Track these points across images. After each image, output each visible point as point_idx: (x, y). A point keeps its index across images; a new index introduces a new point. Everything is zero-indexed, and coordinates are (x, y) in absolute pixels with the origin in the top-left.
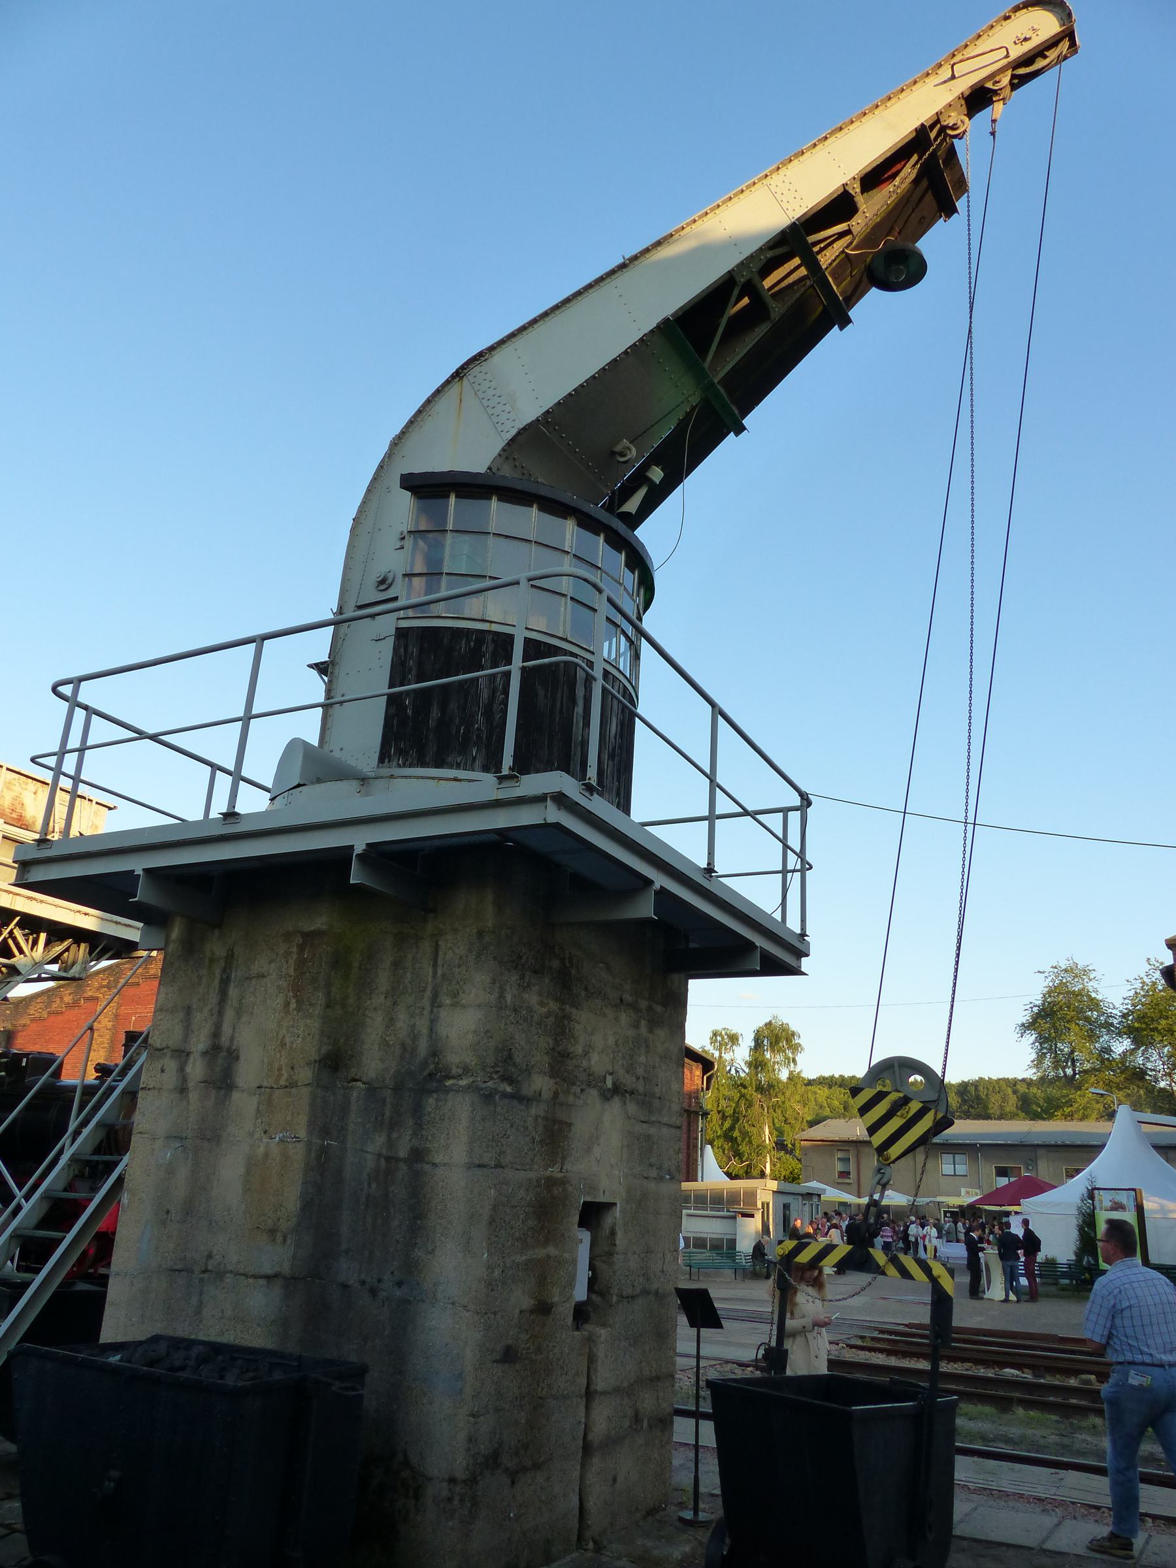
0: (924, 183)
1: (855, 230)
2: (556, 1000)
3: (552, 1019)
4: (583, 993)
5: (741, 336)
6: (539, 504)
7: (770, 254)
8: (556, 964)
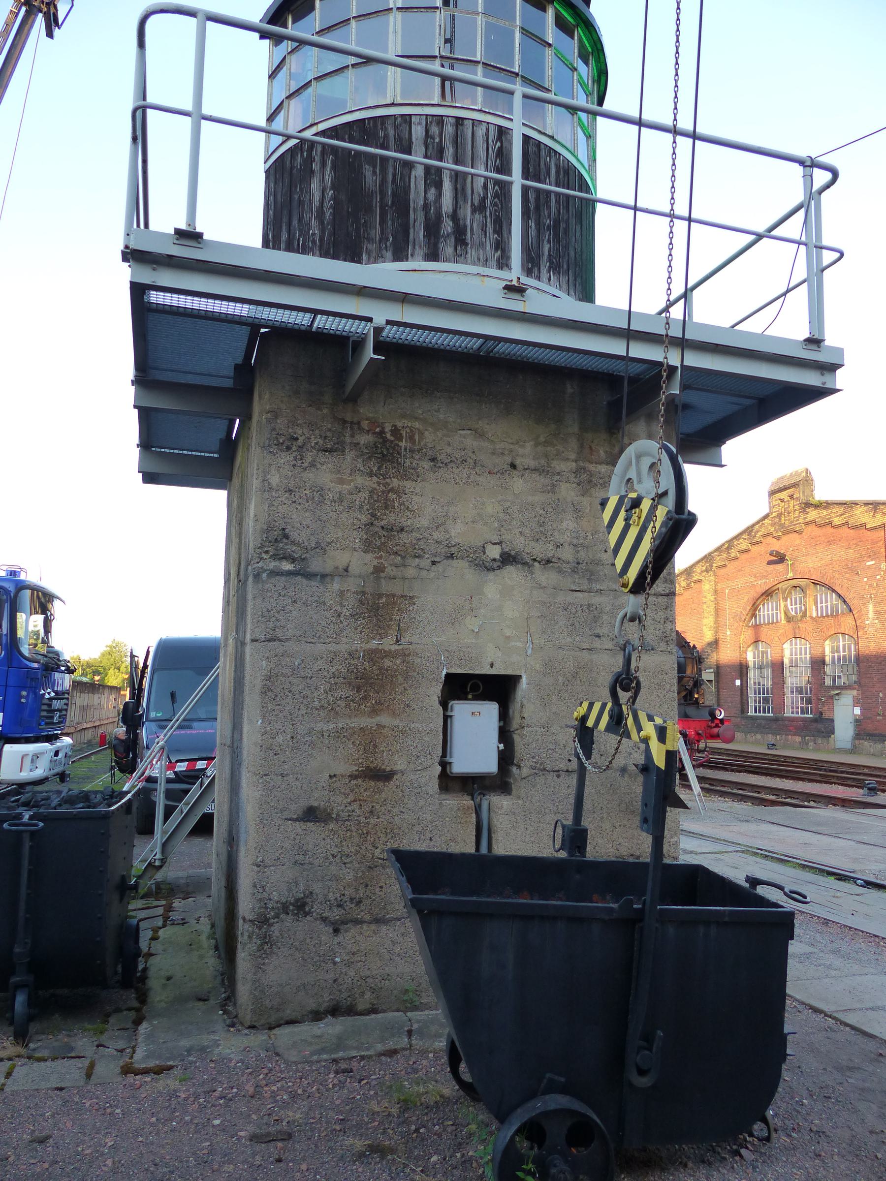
2: (371, 474)
3: (366, 495)
4: (427, 465)
8: (364, 439)
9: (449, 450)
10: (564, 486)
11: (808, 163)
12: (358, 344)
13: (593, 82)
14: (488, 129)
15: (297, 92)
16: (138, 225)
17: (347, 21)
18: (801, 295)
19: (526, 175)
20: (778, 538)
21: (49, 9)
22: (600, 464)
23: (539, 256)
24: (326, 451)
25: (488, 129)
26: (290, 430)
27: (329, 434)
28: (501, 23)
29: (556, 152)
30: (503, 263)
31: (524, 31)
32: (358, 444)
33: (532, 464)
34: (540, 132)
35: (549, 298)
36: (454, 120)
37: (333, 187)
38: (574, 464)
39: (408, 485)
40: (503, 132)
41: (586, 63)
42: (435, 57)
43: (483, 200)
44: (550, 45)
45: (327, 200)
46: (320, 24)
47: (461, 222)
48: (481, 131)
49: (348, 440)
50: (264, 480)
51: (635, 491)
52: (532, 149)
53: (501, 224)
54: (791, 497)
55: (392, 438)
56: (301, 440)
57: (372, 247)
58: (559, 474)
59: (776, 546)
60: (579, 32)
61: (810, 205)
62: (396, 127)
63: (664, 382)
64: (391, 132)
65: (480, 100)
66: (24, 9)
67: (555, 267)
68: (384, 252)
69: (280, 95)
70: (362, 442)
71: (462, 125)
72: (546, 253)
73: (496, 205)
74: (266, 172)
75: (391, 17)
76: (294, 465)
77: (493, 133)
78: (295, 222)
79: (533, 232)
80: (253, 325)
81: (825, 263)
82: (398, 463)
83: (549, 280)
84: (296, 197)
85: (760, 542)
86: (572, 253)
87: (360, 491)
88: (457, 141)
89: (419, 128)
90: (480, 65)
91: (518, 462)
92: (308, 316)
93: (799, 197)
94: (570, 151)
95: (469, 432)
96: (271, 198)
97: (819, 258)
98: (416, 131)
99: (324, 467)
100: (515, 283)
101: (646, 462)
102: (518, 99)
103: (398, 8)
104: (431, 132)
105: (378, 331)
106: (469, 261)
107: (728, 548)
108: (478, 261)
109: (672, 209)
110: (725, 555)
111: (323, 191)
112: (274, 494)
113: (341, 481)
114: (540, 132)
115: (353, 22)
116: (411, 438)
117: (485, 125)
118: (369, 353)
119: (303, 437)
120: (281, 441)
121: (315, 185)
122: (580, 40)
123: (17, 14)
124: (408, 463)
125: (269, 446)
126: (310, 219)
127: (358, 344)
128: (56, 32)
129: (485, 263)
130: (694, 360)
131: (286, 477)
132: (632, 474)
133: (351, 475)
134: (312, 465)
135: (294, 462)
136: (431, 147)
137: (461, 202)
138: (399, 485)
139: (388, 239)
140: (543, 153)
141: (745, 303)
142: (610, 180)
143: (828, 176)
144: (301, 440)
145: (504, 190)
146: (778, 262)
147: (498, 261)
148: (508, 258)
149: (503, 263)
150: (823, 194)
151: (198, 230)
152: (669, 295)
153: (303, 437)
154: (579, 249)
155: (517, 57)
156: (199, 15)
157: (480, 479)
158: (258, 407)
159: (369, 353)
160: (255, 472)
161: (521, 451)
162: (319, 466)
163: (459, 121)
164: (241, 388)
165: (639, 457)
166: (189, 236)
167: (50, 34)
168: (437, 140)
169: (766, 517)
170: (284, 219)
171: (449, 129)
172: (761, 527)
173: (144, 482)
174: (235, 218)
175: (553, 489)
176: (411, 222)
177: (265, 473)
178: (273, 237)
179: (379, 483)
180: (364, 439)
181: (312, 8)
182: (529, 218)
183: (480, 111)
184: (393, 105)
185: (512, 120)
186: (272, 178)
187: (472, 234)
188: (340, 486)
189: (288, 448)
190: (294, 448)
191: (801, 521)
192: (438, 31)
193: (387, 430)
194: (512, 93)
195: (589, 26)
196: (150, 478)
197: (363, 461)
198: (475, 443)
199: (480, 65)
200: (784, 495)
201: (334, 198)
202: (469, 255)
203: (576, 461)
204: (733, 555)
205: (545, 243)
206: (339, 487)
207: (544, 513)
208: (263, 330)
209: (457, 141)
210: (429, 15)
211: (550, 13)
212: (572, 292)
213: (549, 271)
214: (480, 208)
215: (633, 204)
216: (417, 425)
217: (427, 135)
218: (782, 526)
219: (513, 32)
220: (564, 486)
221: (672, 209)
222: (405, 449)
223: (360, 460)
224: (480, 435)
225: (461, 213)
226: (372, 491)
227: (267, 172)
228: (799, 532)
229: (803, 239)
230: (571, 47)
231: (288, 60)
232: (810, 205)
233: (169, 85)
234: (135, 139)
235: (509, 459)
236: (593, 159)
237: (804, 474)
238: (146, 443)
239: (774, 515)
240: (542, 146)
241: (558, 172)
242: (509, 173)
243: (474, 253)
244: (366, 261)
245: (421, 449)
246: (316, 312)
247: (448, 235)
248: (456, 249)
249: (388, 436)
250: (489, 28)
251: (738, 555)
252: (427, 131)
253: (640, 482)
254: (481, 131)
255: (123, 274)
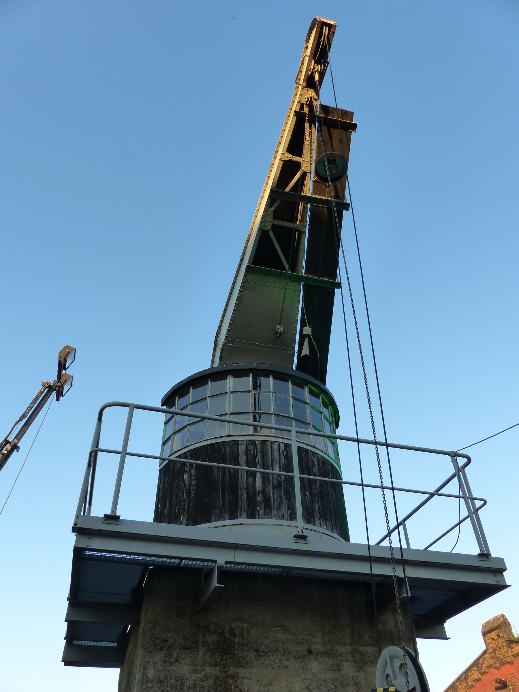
0: (325, 128)
1: (307, 170)
2: (215, 665)
3: (211, 681)
4: (252, 655)
5: (298, 247)
6: (232, 374)
7: (272, 209)
8: (211, 638)
9: (267, 642)
10: (345, 665)
11: (453, 455)
12: (209, 573)
13: (332, 416)
14: (279, 445)
15: (179, 431)
16: (84, 513)
17: (205, 398)
18: (468, 524)
19: (301, 472)
20: (498, 669)
21: (59, 389)
22: (367, 645)
23: (313, 512)
24: (186, 649)
25: (279, 445)
26: (163, 635)
27: (189, 636)
28: (282, 396)
29: (316, 454)
30: (293, 517)
31: (294, 398)
32: (207, 642)
33: (322, 648)
34: (307, 444)
35: (321, 539)
36: (261, 442)
37: (196, 479)
38: (350, 647)
39: (241, 671)
40: (287, 447)
41: (327, 408)
42: (250, 413)
43: (279, 482)
44: (308, 403)
45: (192, 486)
46: (192, 400)
47: (268, 495)
48: (275, 447)
49: (201, 639)
50: (143, 674)
51: (393, 686)
52: (303, 454)
53: (290, 495)
54: (498, 636)
55: (230, 636)
56: (170, 641)
57: (217, 511)
58: (340, 655)
59: (499, 675)
60: (322, 396)
61: (459, 473)
62: (231, 447)
63: (397, 592)
64: (228, 449)
65: (273, 422)
66: (47, 389)
67: (323, 517)
68: (224, 514)
69: (170, 432)
70: (210, 641)
71: (265, 444)
72: (317, 509)
73: (286, 484)
74: (160, 470)
75: (227, 396)
76: (165, 661)
77: (282, 447)
78: (174, 498)
79: (308, 498)
80: (145, 565)
81: (477, 506)
82: (234, 655)
83: (320, 524)
84: (175, 484)
85: (486, 672)
86: (332, 507)
87: (208, 679)
88: (263, 452)
89: (243, 447)
90: (273, 415)
91: (313, 648)
92: (177, 561)
93: (453, 471)
94: (324, 452)
95: (279, 628)
96: (162, 485)
97: (474, 505)
98: (241, 448)
99: (184, 661)
100: (300, 533)
101: (397, 663)
102: (293, 433)
103: (231, 414)
104: (249, 448)
105: (220, 568)
106: (273, 517)
107: (466, 678)
108: (278, 517)
109: (383, 491)
110: (464, 684)
111: (190, 481)
112: (149, 685)
113: (195, 672)
114: (307, 444)
115: (208, 399)
116: (242, 636)
117: (277, 443)
118: (215, 583)
119: (171, 640)
120: (157, 643)
121: (186, 478)
122: (323, 399)
123: (43, 392)
124: (240, 654)
125: (149, 647)
126: (183, 497)
127: (209, 573)
128: (61, 398)
129: (283, 518)
130: (412, 573)
131: (159, 671)
132: (389, 671)
133: (202, 666)
134: (177, 660)
135: (165, 658)
136: (249, 456)
137: (267, 484)
138: (235, 672)
139: (226, 507)
140: (310, 455)
141: (436, 532)
142: (348, 471)
143: (465, 460)
144: (170, 641)
145: (291, 479)
146: (448, 509)
147: (290, 516)
148: (295, 514)
149: (293, 517)
150: (465, 469)
151: (118, 514)
152: (390, 540)
153: (171, 640)
154: (335, 504)
155: (292, 410)
156: (131, 407)
157: (289, 663)
158: (145, 618)
159: (215, 583)
160: (138, 667)
161: (314, 640)
162: (181, 660)
163: (264, 442)
164: (133, 605)
165: (391, 658)
166: (112, 518)
167: (58, 399)
168: (252, 452)
169: (485, 652)
170: (167, 507)
171: (258, 447)
172: (484, 660)
173: (65, 665)
174: (139, 506)
175: (338, 668)
176: (240, 497)
177: (145, 668)
178: (159, 517)
179: (221, 671)
180: (211, 638)
181: (189, 393)
182: (305, 490)
183: (275, 436)
184: (228, 436)
185: (291, 440)
186: (163, 473)
187: (274, 501)
188: (194, 675)
189: (162, 648)
190: (165, 648)
191: (510, 654)
192: (251, 401)
193: (226, 630)
194: (290, 431)
195: (327, 394)
196: (68, 662)
197: (211, 654)
198: (284, 636)
199: (273, 415)
200: (493, 635)
201: (196, 485)
202: (273, 514)
203: (351, 645)
204: (470, 684)
205: (316, 503)
206: (194, 677)
207: (334, 687)
208: (151, 567)
209: (263, 452)
210: (247, 394)
211: (306, 390)
212: (335, 530)
213: (320, 519)
214: (277, 487)
215: (361, 483)
216: (246, 625)
217: (247, 450)
218: (498, 659)
219: (289, 400)
220: (345, 665)
221: (383, 491)
222: (238, 644)
223: (208, 654)
224: (286, 630)
225: (267, 490)
226: (216, 678)
227: (160, 471)
228: (511, 663)
229: (461, 495)
230: (318, 403)
231: (172, 437)
232: (459, 473)
233: (111, 439)
234: (89, 465)
235: (306, 647)
236: (337, 454)
237: (502, 619)
238: (70, 638)
239: (490, 650)
240: (309, 451)
241: (319, 464)
242: (292, 471)
243: (276, 512)
244: (214, 519)
245: (248, 643)
246: (181, 559)
247: (261, 503)
248: (265, 511)
249: (227, 635)
250: (276, 399)
251: (474, 683)
252: (247, 448)
253: (395, 678)
254: (275, 447)
255: (71, 539)
